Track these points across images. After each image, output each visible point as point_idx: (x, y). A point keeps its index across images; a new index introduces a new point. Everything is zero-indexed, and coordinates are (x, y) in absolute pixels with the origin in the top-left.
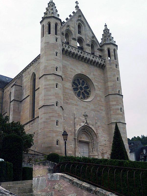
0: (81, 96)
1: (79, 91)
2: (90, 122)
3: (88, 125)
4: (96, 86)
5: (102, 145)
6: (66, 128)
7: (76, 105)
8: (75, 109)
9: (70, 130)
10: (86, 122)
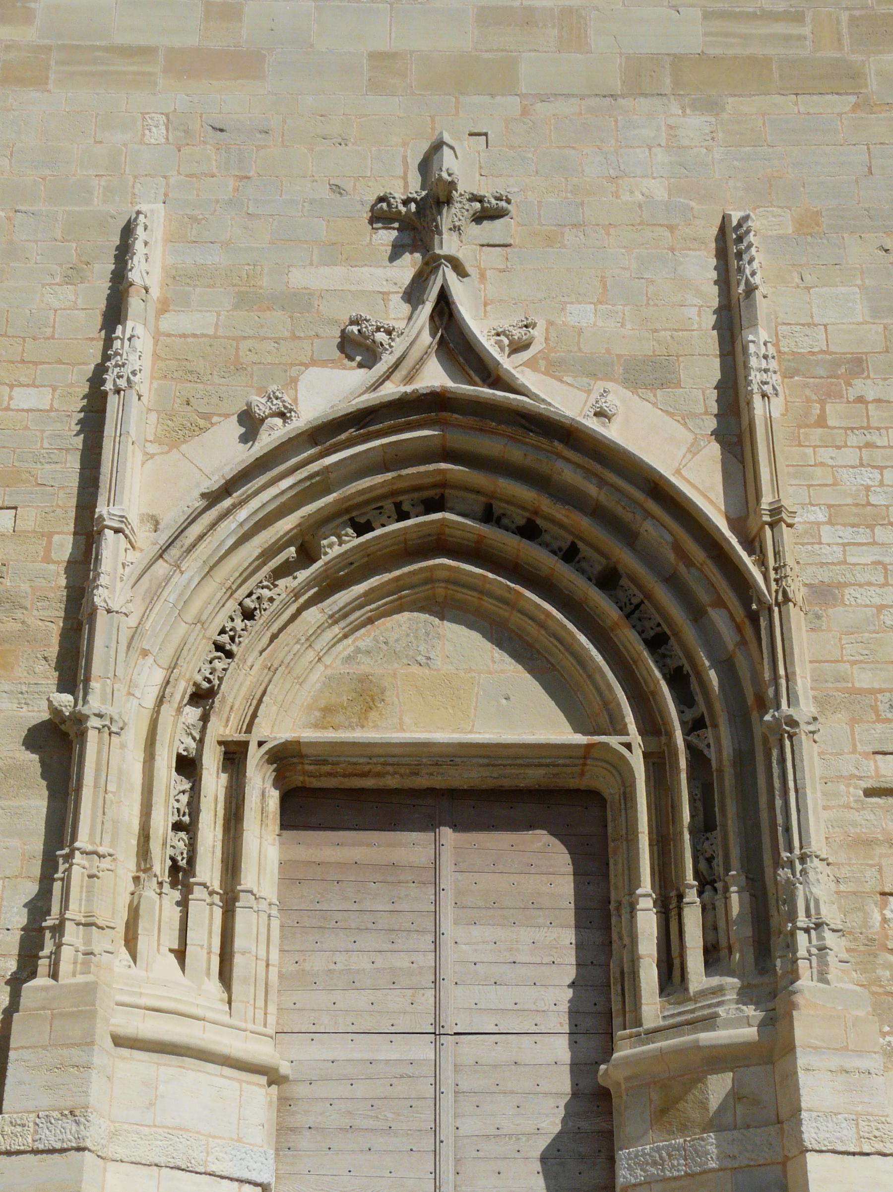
2: (581, 315)
3: (491, 375)
7: (188, 65)
8: (157, 135)
10: (453, 340)
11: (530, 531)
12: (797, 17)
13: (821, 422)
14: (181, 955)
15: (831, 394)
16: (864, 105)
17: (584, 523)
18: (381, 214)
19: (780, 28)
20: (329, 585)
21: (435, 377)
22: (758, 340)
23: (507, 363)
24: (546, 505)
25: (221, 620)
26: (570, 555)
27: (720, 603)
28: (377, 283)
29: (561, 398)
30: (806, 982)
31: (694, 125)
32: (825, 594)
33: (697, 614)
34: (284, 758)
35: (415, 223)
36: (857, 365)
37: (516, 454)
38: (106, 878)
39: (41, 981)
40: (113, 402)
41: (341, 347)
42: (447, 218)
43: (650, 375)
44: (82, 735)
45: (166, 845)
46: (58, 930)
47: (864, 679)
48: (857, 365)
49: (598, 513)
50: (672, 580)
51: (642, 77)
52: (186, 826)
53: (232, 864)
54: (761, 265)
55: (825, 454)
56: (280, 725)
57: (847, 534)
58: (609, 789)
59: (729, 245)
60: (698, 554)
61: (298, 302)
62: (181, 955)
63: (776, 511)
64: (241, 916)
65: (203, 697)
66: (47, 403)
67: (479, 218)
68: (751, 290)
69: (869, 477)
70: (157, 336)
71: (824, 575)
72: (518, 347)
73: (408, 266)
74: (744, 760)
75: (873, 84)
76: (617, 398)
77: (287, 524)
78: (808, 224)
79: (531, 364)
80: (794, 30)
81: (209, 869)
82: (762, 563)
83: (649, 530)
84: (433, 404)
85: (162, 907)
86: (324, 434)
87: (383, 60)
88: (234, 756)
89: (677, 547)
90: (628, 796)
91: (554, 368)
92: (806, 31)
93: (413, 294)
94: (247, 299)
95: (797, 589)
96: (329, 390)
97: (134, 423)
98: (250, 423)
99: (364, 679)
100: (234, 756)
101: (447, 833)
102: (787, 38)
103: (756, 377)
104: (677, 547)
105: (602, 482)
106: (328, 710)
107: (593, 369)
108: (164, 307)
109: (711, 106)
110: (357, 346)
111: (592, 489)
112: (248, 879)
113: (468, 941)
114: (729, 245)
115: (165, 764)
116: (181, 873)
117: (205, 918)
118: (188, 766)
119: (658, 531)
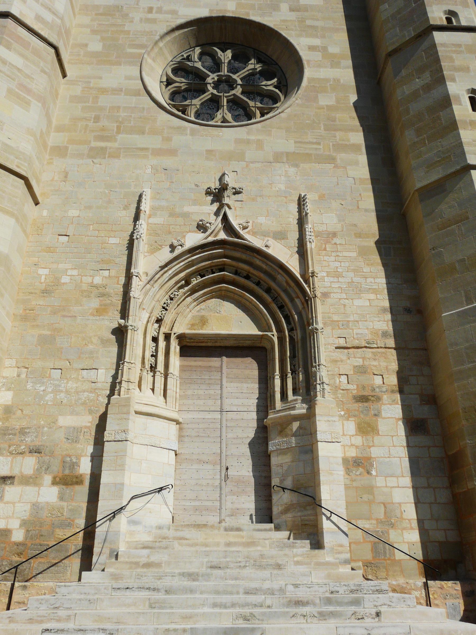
0: (224, 112)
1: (206, 97)
2: (262, 220)
3: (238, 236)
4: (312, 48)
5: (356, 343)
6: (65, 279)
7: (158, 152)
8: (149, 171)
9: (96, 287)
11: (247, 277)
12: (319, 144)
13: (325, 249)
14: (153, 390)
15: (327, 242)
16: (336, 167)
17: (262, 275)
18: (208, 192)
19: (314, 146)
20: (193, 291)
21: (222, 236)
22: (308, 227)
23: (242, 232)
24: (252, 270)
25: (164, 300)
26: (258, 284)
27: (298, 297)
28: (207, 211)
29: (256, 242)
30: (319, 398)
31: (292, 170)
32: (326, 295)
33: (292, 300)
34: (181, 338)
35: (218, 195)
36: (334, 235)
37: (244, 257)
38: (133, 369)
39: (116, 396)
40: (136, 241)
41: (197, 227)
42: (226, 194)
43: (280, 236)
44: (127, 331)
45: (149, 360)
46: (120, 383)
47: (335, 318)
48: (334, 235)
49: (265, 272)
50: (285, 291)
51: (278, 158)
52: (155, 356)
53: (167, 366)
54: (309, 207)
55: (326, 258)
56: (180, 329)
57: (332, 279)
58: (268, 347)
59: (301, 202)
60: (292, 284)
61: (186, 215)
62: (153, 390)
63: (313, 273)
64: (169, 380)
65: (159, 321)
66: (118, 242)
67: (234, 194)
68: (307, 214)
69: (337, 264)
70: (148, 224)
71: (325, 290)
72: (245, 228)
73: (215, 206)
74: (304, 339)
75: (339, 161)
76: (271, 242)
77: (182, 275)
78: (322, 197)
79: (248, 233)
80: (318, 147)
81: (160, 367)
82: (309, 287)
83: (279, 277)
84: (222, 243)
85: (148, 377)
86: (192, 251)
87: (209, 152)
88: (167, 337)
89: (287, 282)
90: (273, 348)
91: (254, 234)
92: (321, 147)
93: (217, 214)
94: (172, 214)
95: (318, 294)
96: (194, 239)
97: (141, 248)
98: (173, 248)
99: (203, 317)
100: (167, 337)
101: (224, 358)
102: (316, 149)
103: (308, 237)
104: (287, 282)
105: (267, 265)
106: (193, 325)
107: (265, 234)
108: (150, 216)
109: (297, 166)
110: (202, 227)
111: (264, 266)
112: (171, 370)
113: (230, 387)
114: (301, 202)
115: (149, 339)
116: (153, 368)
117: (160, 380)
118: (155, 340)
119: (281, 278)
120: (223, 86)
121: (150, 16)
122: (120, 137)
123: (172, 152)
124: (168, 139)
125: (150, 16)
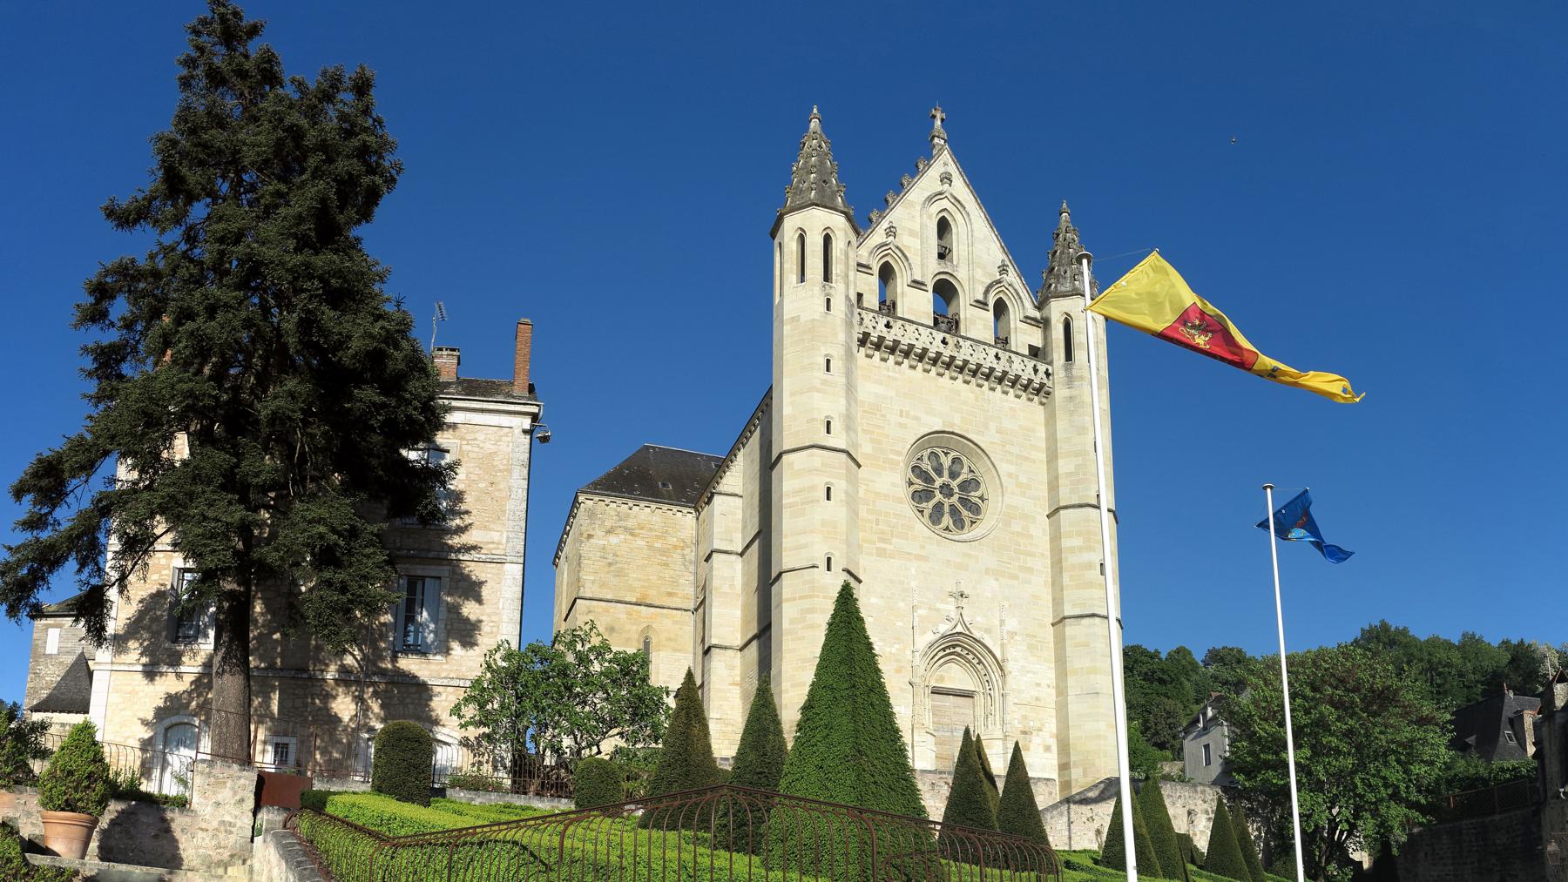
0: (947, 520)
4: (1010, 475)
31: (995, 583)
120: (945, 491)
121: (903, 420)
122: (894, 540)
123: (924, 559)
124: (923, 547)
125: (903, 420)
